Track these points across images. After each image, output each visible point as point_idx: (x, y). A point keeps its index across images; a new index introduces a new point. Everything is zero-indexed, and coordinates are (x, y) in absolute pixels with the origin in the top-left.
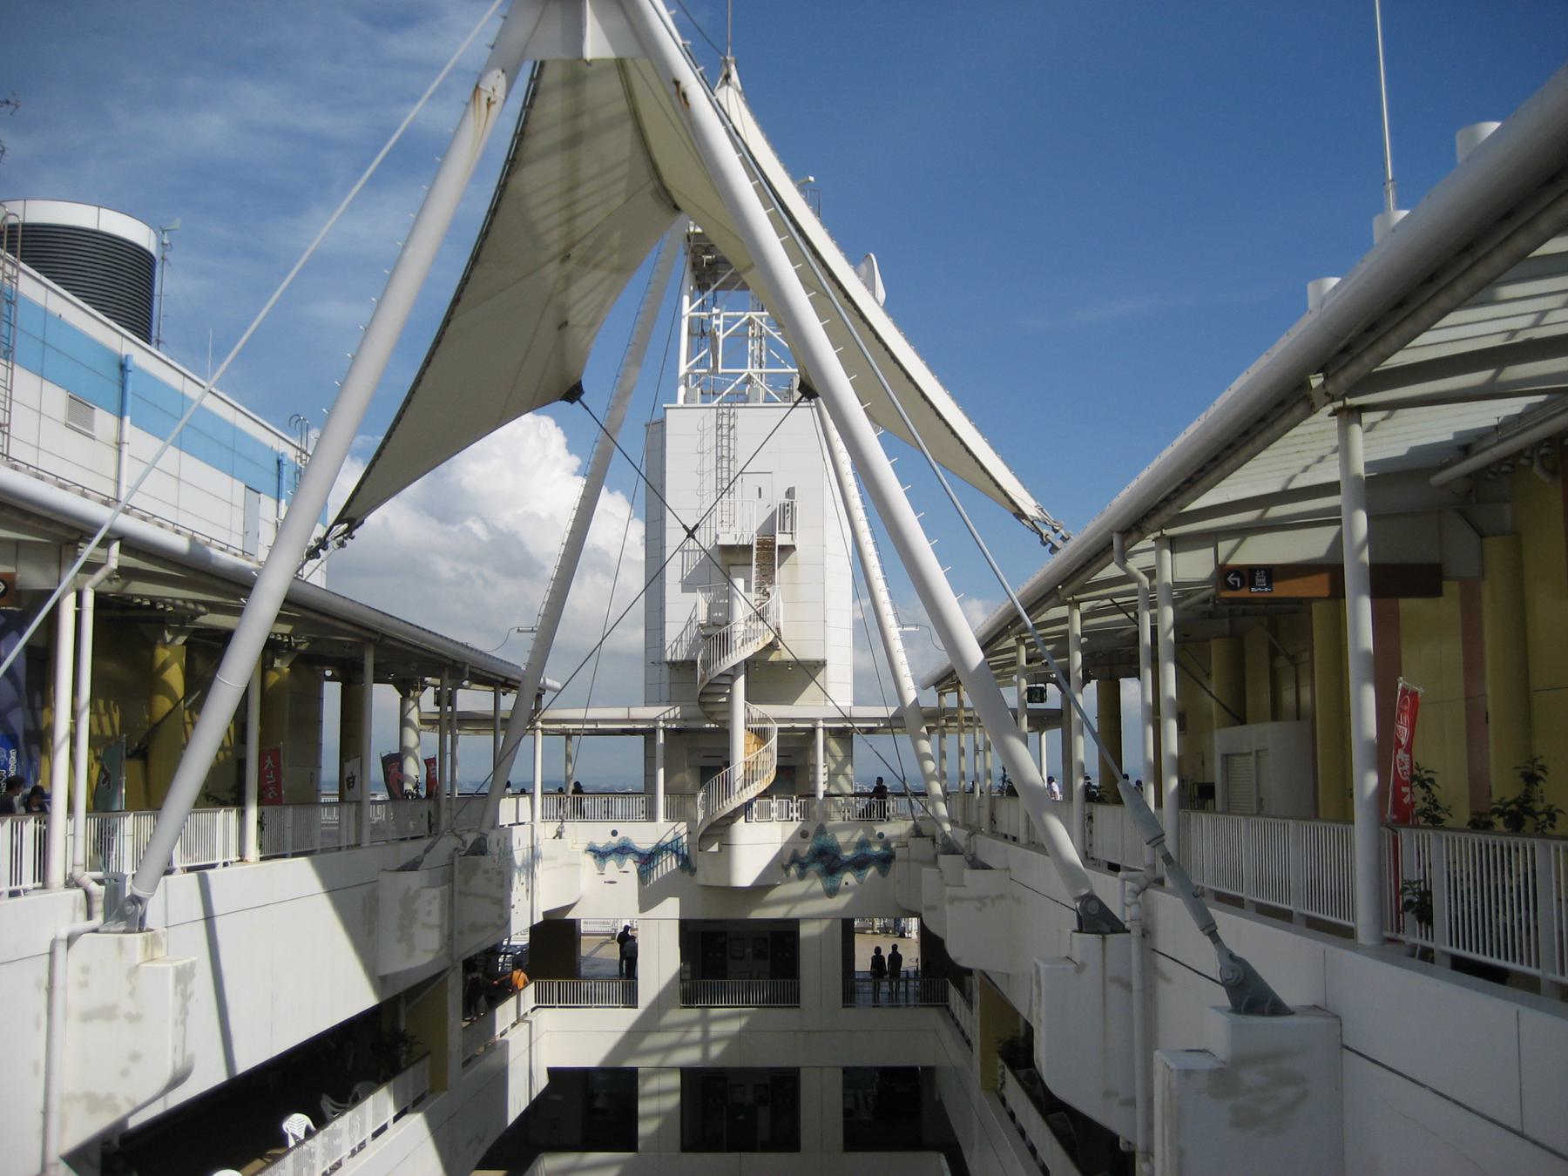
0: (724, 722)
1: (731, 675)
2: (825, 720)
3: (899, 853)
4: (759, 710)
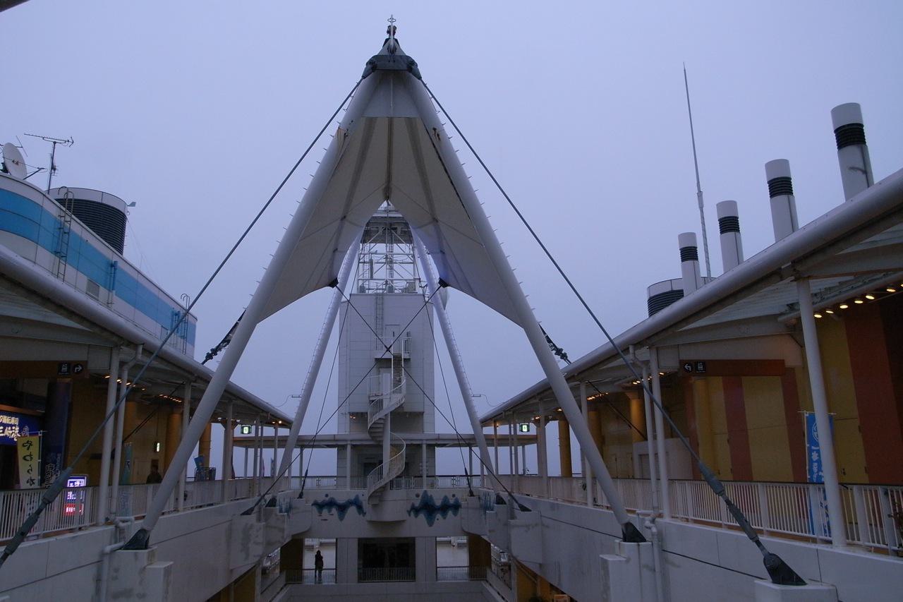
0: (380, 441)
1: (384, 419)
2: (427, 440)
3: (463, 503)
4: (398, 435)
